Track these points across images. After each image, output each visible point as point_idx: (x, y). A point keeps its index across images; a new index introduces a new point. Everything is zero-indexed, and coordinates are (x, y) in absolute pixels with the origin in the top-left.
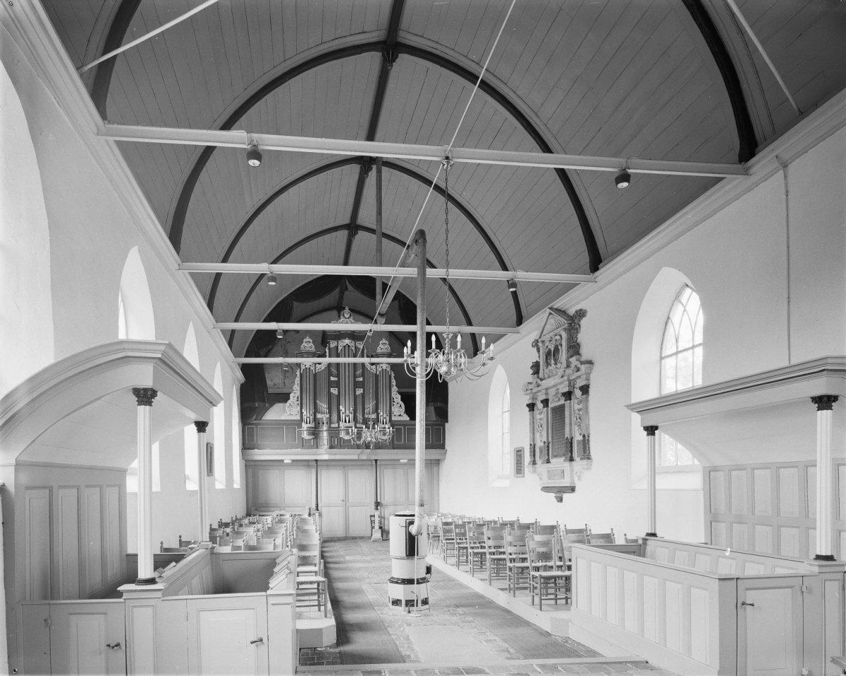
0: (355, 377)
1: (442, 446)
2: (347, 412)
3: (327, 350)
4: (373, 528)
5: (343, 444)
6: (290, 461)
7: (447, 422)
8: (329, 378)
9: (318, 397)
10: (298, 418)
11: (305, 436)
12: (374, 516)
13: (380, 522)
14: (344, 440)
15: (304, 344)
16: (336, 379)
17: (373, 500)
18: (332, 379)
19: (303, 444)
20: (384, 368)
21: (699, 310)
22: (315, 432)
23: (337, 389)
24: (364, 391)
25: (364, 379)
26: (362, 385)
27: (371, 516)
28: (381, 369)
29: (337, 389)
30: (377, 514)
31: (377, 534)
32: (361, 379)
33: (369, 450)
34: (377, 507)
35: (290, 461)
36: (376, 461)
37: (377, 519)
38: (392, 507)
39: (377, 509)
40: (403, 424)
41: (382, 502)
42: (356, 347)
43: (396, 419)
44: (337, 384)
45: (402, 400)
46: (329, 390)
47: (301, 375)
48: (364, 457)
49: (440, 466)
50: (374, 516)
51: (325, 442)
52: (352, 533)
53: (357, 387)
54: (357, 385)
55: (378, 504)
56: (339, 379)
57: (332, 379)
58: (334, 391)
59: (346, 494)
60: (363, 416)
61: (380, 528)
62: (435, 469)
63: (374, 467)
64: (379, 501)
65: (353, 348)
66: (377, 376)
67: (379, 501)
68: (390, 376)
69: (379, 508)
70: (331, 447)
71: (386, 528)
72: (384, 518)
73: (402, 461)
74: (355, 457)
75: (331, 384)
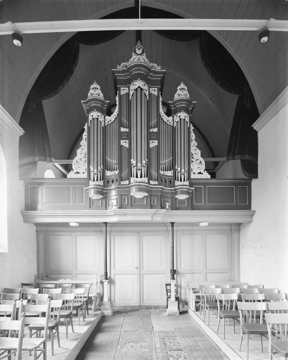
0: (149, 127)
1: (248, 207)
2: (139, 164)
3: (117, 98)
4: (168, 298)
5: (133, 203)
6: (77, 225)
7: (256, 177)
8: (119, 129)
9: (108, 153)
10: (85, 176)
11: (95, 197)
12: (170, 285)
13: (177, 292)
14: (135, 198)
15: (90, 92)
16: (127, 130)
17: (169, 268)
18: (123, 130)
19: (91, 203)
20: (182, 117)
21: (115, 278)
22: (103, 192)
23: (127, 141)
24: (159, 143)
25: (159, 130)
26: (157, 135)
27: (167, 285)
28: (178, 120)
29: (127, 141)
30: (173, 283)
31: (173, 307)
32: (155, 130)
33: (164, 210)
34: (173, 276)
35: (77, 225)
36: (173, 224)
37: (173, 288)
38: (188, 276)
39: (174, 279)
40: (203, 183)
41: (179, 270)
42: (150, 94)
43: (196, 177)
44: (128, 135)
45: (202, 156)
46: (119, 142)
47: (89, 128)
48: (158, 219)
49: (241, 232)
50: (170, 285)
51: (114, 202)
52: (147, 303)
53: (151, 139)
54: (150, 137)
55: (174, 272)
56: (130, 130)
57: (123, 130)
58: (125, 144)
59: (141, 261)
60: (158, 172)
61: (177, 299)
62: (236, 235)
63: (170, 233)
64: (175, 269)
65: (147, 93)
66: (173, 129)
67: (175, 269)
68: (189, 129)
69: (175, 276)
70: (121, 207)
71: (183, 297)
72: (181, 287)
73: (201, 224)
74: (148, 219)
75: (121, 136)
